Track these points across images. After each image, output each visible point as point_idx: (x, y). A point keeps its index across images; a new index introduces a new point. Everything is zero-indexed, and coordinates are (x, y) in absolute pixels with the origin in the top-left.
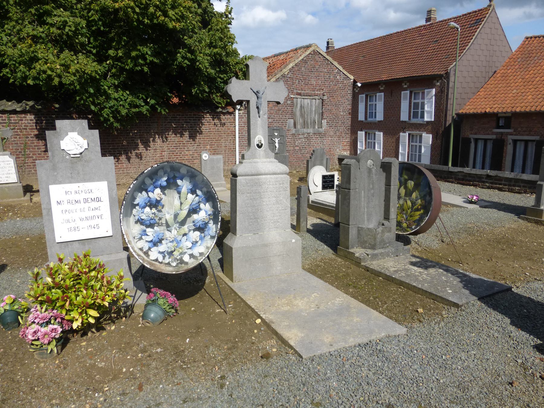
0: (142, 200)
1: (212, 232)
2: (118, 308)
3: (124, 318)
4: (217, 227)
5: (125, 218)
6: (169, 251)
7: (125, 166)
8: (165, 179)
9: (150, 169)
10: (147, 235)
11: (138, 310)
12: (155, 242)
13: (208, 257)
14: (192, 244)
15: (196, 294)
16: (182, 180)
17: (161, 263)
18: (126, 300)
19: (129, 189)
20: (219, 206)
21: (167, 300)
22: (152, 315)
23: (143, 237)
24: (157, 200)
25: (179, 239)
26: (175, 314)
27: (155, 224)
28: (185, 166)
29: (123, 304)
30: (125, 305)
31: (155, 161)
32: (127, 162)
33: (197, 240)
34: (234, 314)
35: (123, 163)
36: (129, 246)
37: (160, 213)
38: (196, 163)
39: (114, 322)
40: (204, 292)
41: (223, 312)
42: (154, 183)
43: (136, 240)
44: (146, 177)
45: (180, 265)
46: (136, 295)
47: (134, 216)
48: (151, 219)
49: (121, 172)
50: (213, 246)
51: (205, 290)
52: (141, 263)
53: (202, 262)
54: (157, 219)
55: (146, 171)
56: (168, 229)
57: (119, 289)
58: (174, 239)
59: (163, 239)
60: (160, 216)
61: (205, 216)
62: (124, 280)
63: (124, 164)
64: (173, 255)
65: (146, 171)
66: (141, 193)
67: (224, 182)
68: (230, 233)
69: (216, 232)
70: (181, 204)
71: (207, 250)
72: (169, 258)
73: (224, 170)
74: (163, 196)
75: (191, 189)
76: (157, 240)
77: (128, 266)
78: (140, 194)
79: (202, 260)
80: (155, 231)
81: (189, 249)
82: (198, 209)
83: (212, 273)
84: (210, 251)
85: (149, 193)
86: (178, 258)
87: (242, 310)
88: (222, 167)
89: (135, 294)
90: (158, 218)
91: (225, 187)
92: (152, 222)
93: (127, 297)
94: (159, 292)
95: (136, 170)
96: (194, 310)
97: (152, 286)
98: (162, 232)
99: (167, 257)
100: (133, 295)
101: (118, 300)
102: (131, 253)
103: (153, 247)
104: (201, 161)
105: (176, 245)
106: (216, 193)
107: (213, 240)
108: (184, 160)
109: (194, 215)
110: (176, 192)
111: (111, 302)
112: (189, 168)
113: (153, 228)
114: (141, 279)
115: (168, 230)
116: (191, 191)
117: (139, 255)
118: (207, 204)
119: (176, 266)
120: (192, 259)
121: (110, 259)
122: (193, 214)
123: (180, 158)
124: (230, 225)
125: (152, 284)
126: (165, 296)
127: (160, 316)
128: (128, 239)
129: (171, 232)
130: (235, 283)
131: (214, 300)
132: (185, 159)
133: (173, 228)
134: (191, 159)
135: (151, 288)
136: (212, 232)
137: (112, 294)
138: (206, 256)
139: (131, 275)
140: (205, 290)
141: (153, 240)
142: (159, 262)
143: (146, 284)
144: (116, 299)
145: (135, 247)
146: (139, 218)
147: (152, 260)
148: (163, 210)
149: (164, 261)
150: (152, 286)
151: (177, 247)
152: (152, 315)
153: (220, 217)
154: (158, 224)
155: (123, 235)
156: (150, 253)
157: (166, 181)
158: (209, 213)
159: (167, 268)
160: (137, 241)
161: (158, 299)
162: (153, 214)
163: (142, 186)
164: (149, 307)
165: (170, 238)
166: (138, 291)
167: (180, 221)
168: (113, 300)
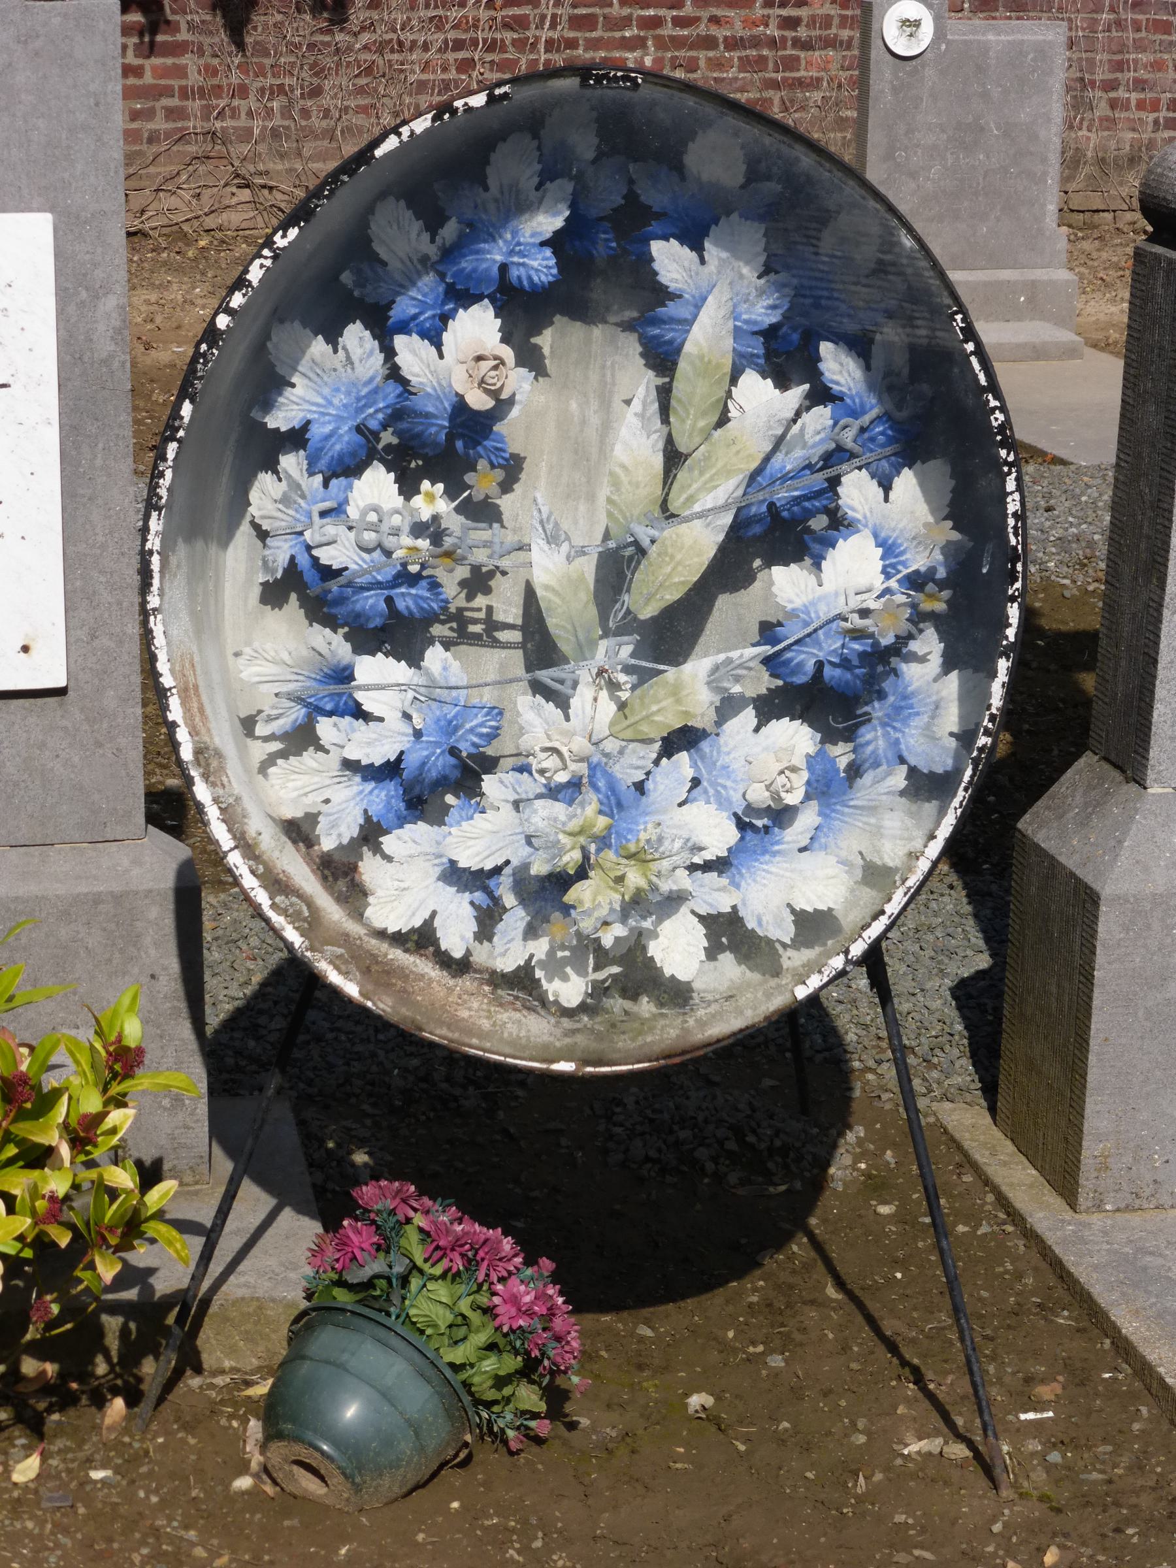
0: (340, 399)
1: (929, 733)
2: (72, 1309)
3: (119, 1403)
4: (973, 698)
5: (181, 551)
6: (539, 868)
7: (194, 78)
8: (549, 222)
9: (421, 125)
10: (360, 713)
11: (232, 1351)
12: (418, 779)
13: (873, 960)
14: (742, 826)
15: (740, 1273)
16: (697, 247)
17: (460, 967)
18: (141, 1256)
19: (237, 300)
20: (1013, 506)
21: (483, 1299)
22: (351, 1412)
23: (325, 728)
24: (460, 407)
25: (627, 771)
26: (541, 1427)
27: (431, 618)
28: (732, 121)
29: (120, 1282)
30: (131, 1294)
31: (459, 45)
32: (223, 36)
33: (792, 799)
34: (1064, 1495)
35: (178, 49)
36: (202, 792)
37: (482, 534)
38: (815, 84)
39: (36, 1428)
40: (807, 1267)
41: (962, 1465)
42: (450, 253)
43: (259, 751)
44: (382, 195)
45: (617, 1004)
46: (231, 1224)
47: (263, 535)
48: (405, 578)
49: (160, 124)
50: (924, 865)
51: (816, 1244)
52: (289, 946)
53: (814, 1000)
54: (451, 581)
55: (392, 143)
56: (544, 675)
57: (97, 1154)
58: (582, 769)
59: (490, 764)
60: (480, 556)
61: (879, 583)
62: (142, 1082)
63: (188, 60)
64: (567, 909)
65: (392, 143)
66: (333, 338)
67: (1063, 275)
68: (1086, 761)
69: (966, 738)
70: (673, 458)
71: (869, 895)
72: (531, 932)
73: (1072, 161)
74: (518, 381)
75: (769, 334)
76: (440, 763)
77: (173, 965)
78: (319, 346)
79: (815, 982)
80: (432, 685)
81: (707, 867)
82: (819, 523)
83: (890, 1099)
84: (892, 908)
85: (400, 341)
86: (607, 941)
87: (1138, 1467)
88: (1052, 136)
89: (223, 1212)
90: (463, 572)
91: (1060, 321)
92: (407, 599)
93: (154, 1229)
94: (419, 1220)
95: (286, 112)
96: (709, 1417)
97: (360, 1158)
98: (488, 697)
99: (516, 918)
100: (206, 1217)
101: (81, 1245)
102: (218, 858)
103: (401, 822)
104: (864, 63)
105: (602, 822)
106: (993, 387)
107: (930, 807)
108: (709, 42)
109: (777, 572)
110: (631, 346)
111: (28, 1253)
112: (769, 140)
113: (414, 660)
114: (279, 1091)
115: (538, 688)
116: (769, 354)
117: (276, 884)
118: (906, 482)
119: (583, 1008)
120: (727, 959)
121: (30, 889)
122: (769, 563)
123: (679, 22)
124: (1088, 681)
125: (361, 1143)
126: (471, 1263)
127: (416, 1428)
128: (193, 732)
129: (563, 703)
130: (1096, 1219)
131: (892, 1347)
132: (720, 33)
133: (585, 676)
134: (772, 43)
135: (356, 1178)
136: (929, 733)
137: (34, 1193)
138: (857, 949)
139: (191, 1042)
140: (816, 1244)
141: (411, 763)
142: (444, 961)
143: (310, 1138)
144: (64, 1240)
145: (249, 805)
146: (303, 561)
147: (382, 934)
148: (506, 503)
149: (482, 955)
150: (360, 1158)
151: (603, 842)
152: (351, 1412)
153: (1013, 612)
154: (460, 619)
155: (155, 694)
156: (370, 868)
157: (555, 242)
158: (918, 561)
159: (504, 1016)
160: (270, 760)
161: (405, 1281)
162: (419, 529)
163: (346, 278)
164: (326, 1340)
165: (551, 762)
166: (249, 1190)
167: (647, 612)
168: (42, 1244)
